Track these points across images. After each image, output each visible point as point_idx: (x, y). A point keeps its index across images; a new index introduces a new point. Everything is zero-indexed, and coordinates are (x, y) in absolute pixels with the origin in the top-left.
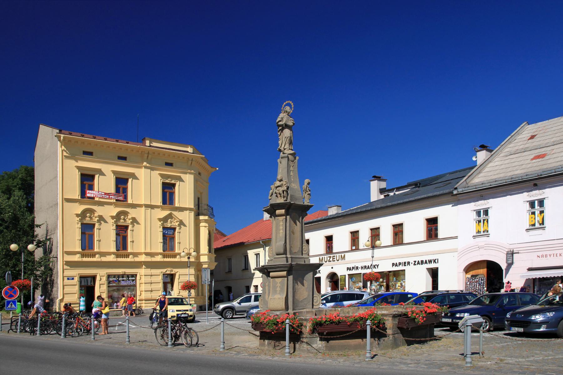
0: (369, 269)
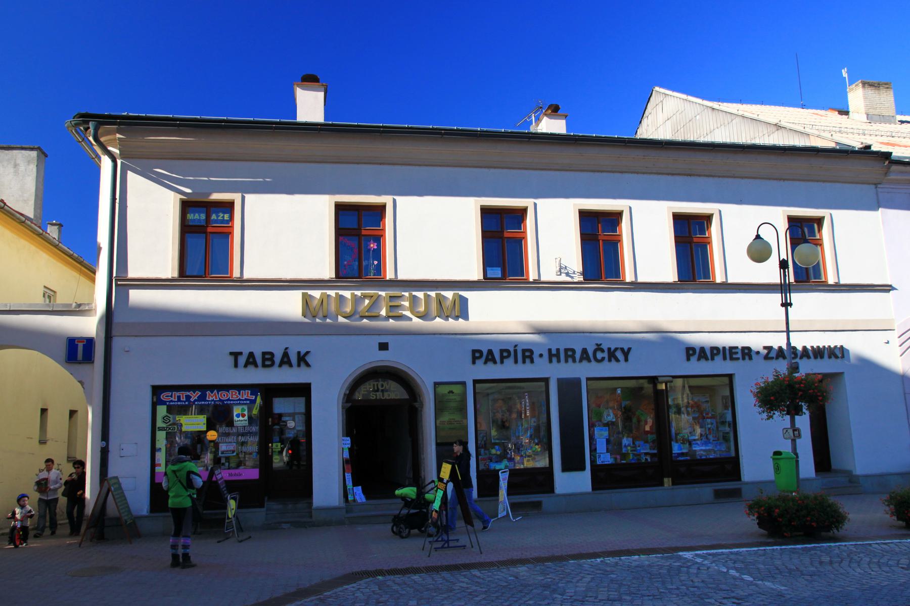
0: (589, 361)
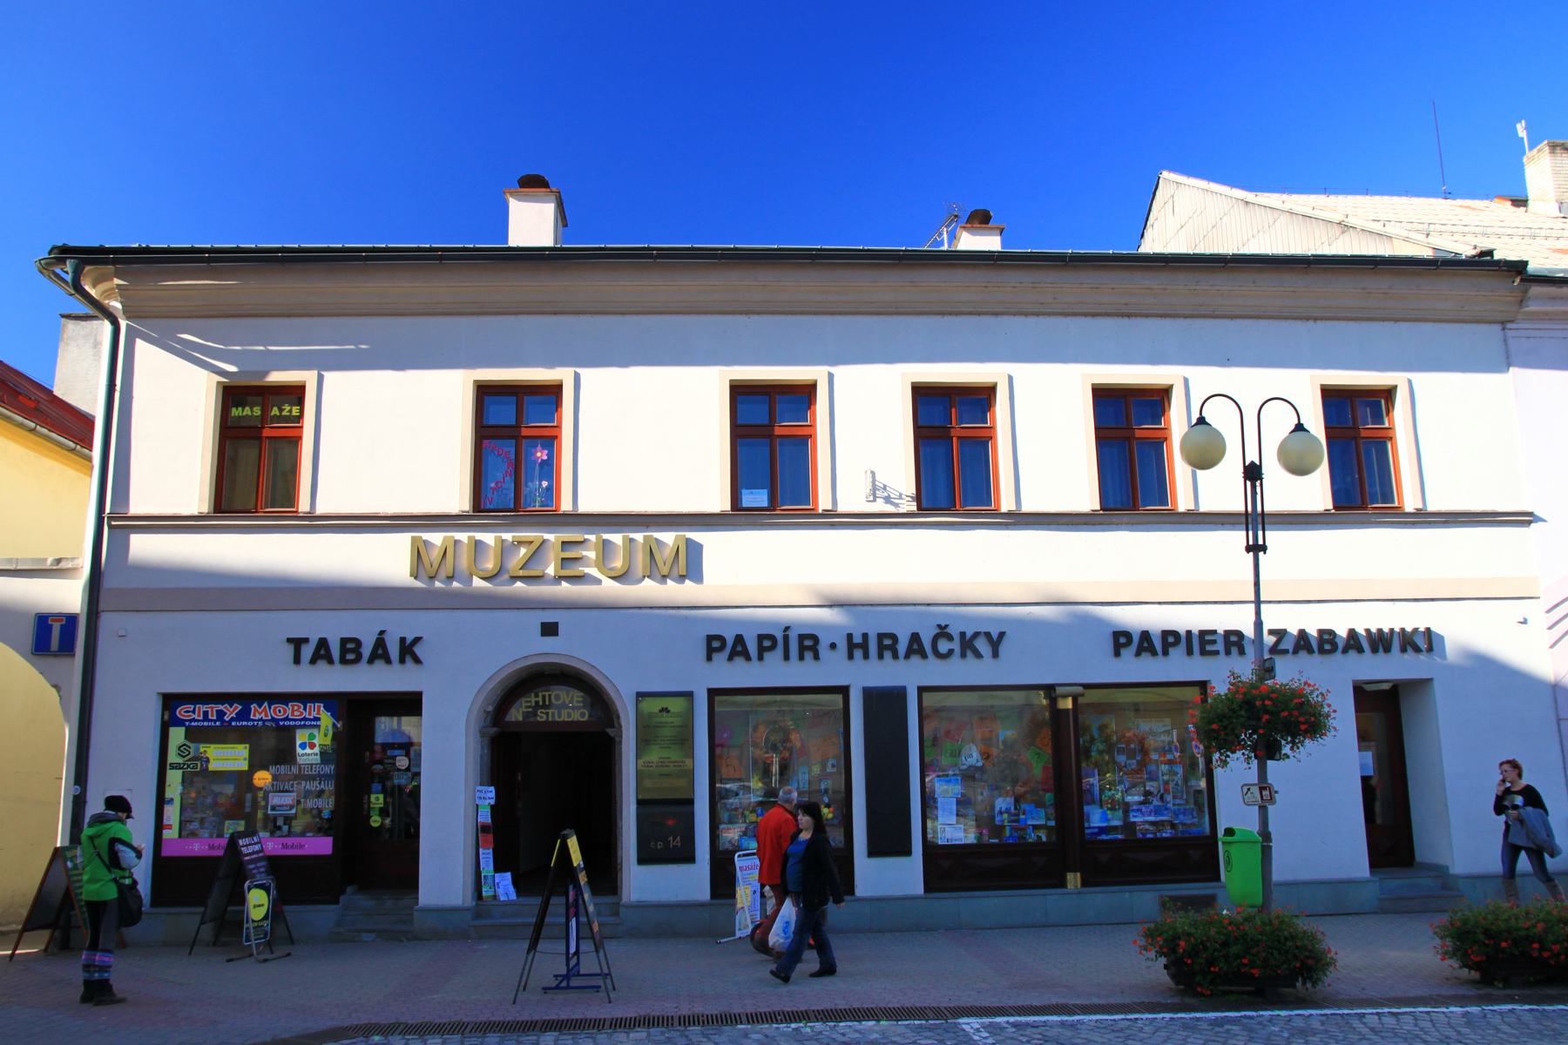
0: (924, 656)
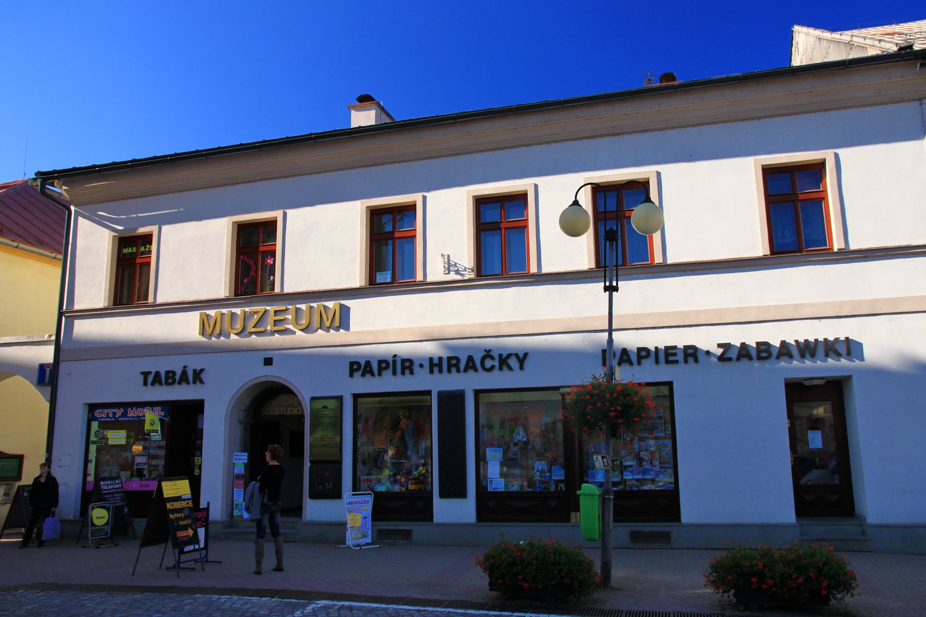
0: (476, 370)
